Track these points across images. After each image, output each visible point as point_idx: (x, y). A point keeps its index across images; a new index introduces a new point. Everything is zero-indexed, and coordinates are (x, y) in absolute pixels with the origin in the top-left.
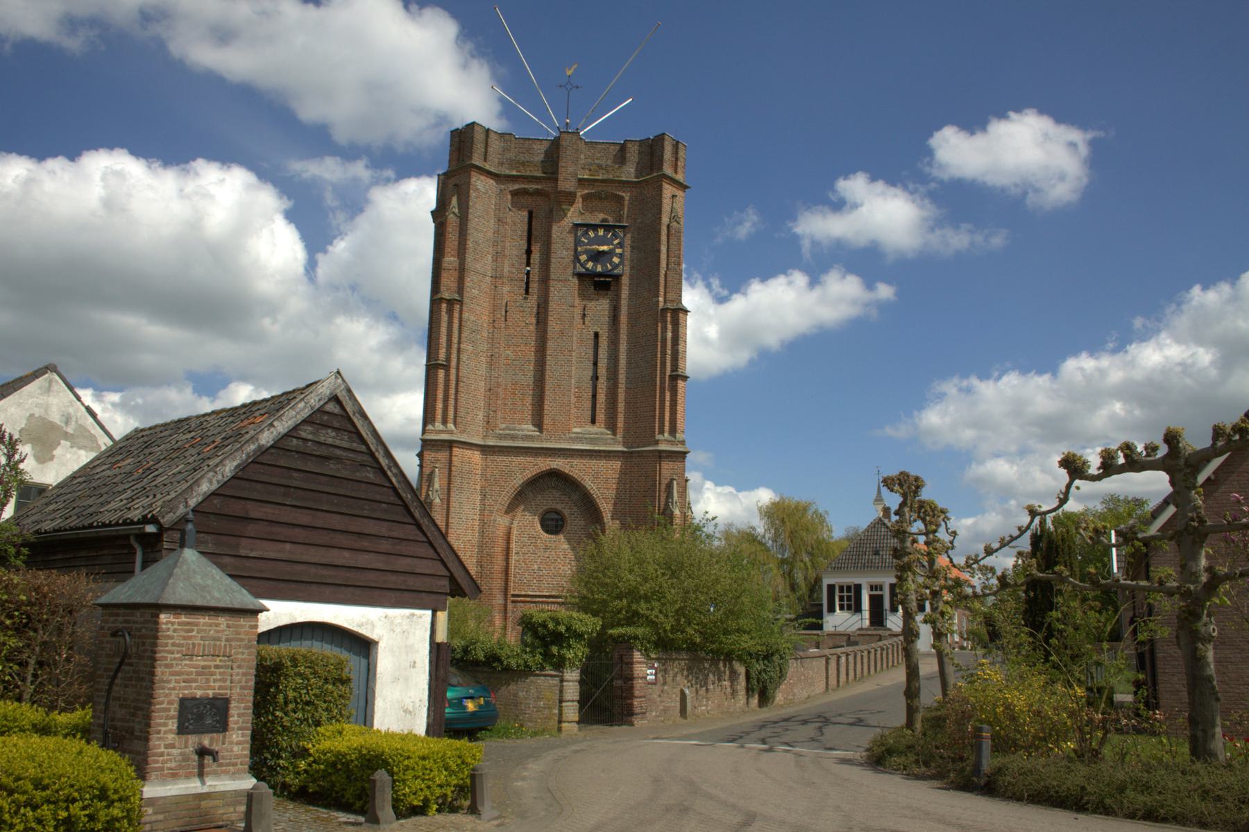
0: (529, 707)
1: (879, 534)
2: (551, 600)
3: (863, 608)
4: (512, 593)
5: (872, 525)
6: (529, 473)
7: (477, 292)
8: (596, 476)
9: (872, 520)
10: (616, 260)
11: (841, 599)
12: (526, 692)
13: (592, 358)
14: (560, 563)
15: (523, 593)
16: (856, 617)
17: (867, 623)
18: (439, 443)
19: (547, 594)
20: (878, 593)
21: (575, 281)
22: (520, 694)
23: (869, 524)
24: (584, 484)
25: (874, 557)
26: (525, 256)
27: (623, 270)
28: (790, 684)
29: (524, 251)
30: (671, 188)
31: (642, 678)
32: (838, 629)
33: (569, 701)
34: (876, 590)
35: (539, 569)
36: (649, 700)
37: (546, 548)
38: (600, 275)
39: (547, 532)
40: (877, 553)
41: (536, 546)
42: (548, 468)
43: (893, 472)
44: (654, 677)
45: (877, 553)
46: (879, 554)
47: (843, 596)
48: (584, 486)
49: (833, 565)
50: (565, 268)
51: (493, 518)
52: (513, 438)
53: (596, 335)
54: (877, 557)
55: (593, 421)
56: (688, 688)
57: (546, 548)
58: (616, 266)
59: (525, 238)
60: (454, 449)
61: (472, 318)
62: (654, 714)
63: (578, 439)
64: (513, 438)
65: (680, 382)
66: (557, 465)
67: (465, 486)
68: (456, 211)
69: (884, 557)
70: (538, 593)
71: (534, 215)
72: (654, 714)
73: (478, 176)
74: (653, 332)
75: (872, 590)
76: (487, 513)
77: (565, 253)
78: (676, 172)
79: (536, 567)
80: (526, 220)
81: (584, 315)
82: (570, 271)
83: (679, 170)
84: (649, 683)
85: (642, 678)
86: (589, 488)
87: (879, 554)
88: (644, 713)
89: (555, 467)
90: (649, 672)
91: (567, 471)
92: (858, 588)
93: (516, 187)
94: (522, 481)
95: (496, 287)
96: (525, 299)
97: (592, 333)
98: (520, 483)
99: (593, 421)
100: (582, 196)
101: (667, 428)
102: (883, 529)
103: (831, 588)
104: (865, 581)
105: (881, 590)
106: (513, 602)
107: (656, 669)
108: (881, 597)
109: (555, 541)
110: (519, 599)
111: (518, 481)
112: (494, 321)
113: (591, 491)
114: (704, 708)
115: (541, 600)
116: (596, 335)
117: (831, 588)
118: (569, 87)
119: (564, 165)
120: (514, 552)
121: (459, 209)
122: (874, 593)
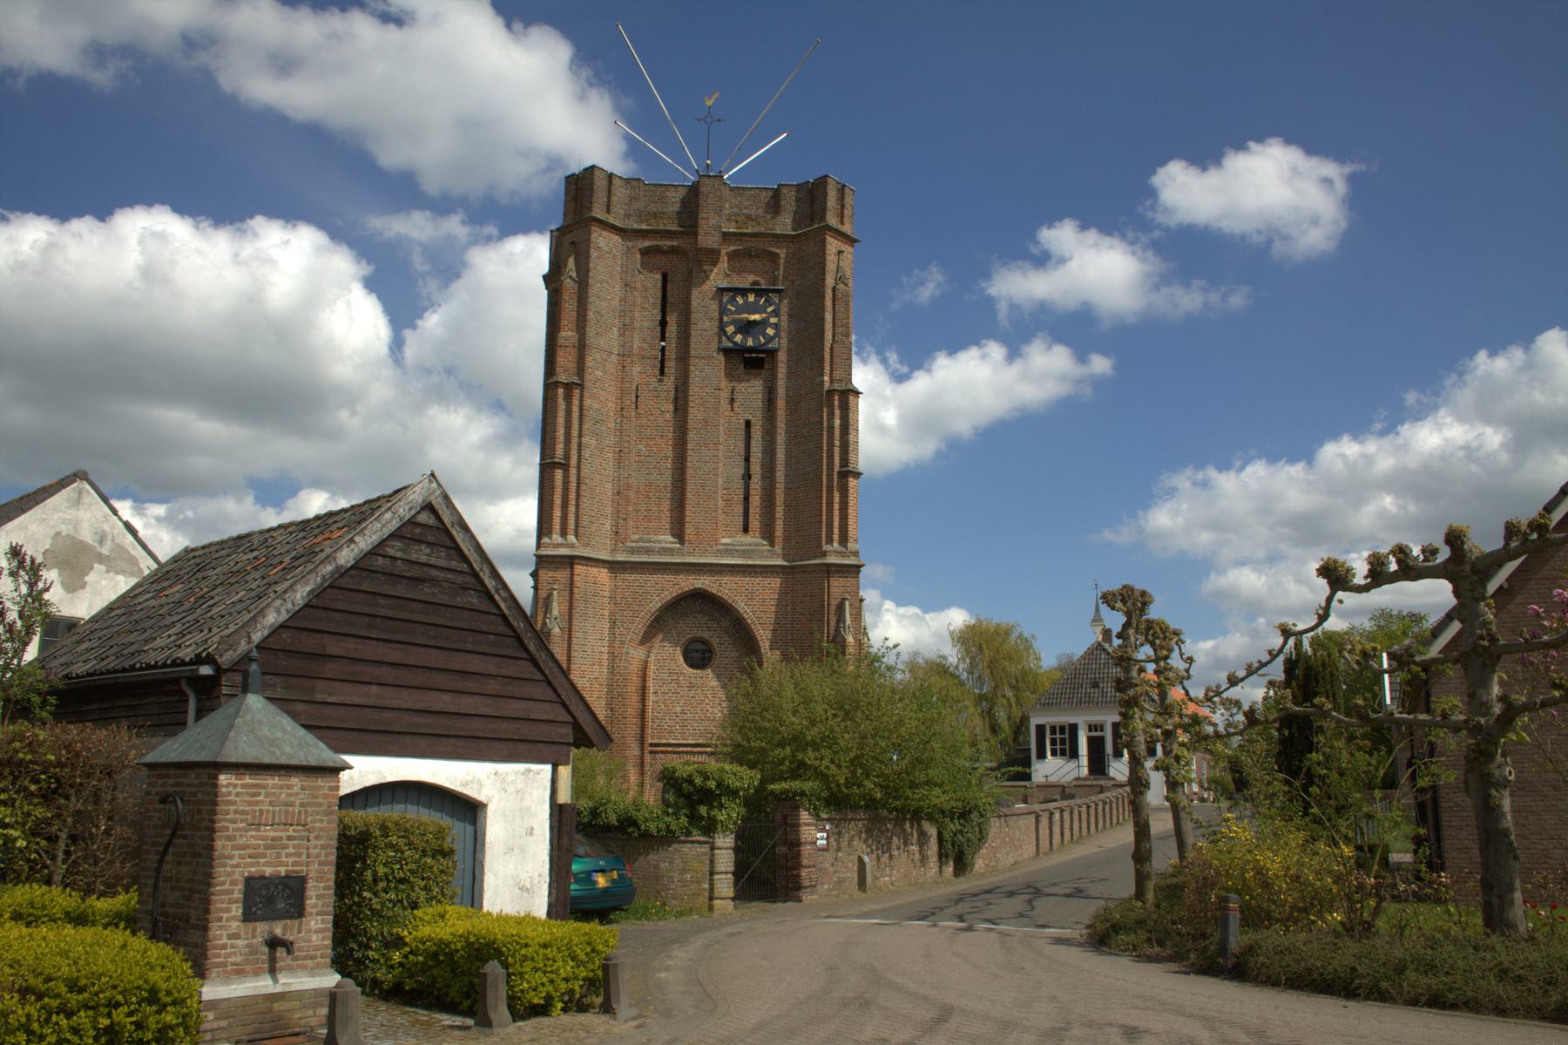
3: (1080, 753)
4: (650, 741)
6: (668, 595)
7: (601, 374)
8: (750, 597)
12: (670, 862)
15: (664, 741)
16: (1072, 764)
17: (1085, 771)
19: (693, 742)
20: (1099, 734)
21: (721, 358)
22: (662, 865)
23: (1085, 650)
26: (659, 329)
29: (658, 323)
30: (836, 242)
31: (810, 843)
32: (1050, 779)
33: (722, 873)
34: (1096, 730)
35: (683, 712)
36: (821, 869)
38: (751, 350)
39: (692, 666)
40: (1095, 685)
42: (691, 588)
44: (825, 842)
45: (1095, 685)
46: (1098, 687)
50: (708, 343)
52: (648, 551)
53: (748, 424)
54: (1096, 690)
55: (746, 530)
57: (691, 686)
59: (659, 307)
60: (576, 566)
62: (826, 887)
63: (729, 552)
64: (648, 551)
66: (703, 584)
68: (574, 274)
71: (669, 278)
72: (826, 887)
74: (818, 419)
78: (842, 222)
79: (678, 709)
81: (732, 400)
82: (714, 346)
83: (846, 220)
84: (820, 850)
85: (810, 843)
86: (742, 612)
87: (1098, 687)
88: (815, 886)
90: (819, 835)
92: (1074, 729)
93: (647, 243)
94: (660, 604)
95: (624, 367)
98: (658, 606)
99: (746, 530)
102: (1103, 656)
103: (1041, 729)
104: (1081, 720)
105: (1102, 730)
107: (827, 832)
108: (1102, 739)
110: (658, 749)
111: (655, 604)
114: (887, 879)
115: (685, 749)
117: (1041, 729)
119: (704, 216)
122: (1094, 734)
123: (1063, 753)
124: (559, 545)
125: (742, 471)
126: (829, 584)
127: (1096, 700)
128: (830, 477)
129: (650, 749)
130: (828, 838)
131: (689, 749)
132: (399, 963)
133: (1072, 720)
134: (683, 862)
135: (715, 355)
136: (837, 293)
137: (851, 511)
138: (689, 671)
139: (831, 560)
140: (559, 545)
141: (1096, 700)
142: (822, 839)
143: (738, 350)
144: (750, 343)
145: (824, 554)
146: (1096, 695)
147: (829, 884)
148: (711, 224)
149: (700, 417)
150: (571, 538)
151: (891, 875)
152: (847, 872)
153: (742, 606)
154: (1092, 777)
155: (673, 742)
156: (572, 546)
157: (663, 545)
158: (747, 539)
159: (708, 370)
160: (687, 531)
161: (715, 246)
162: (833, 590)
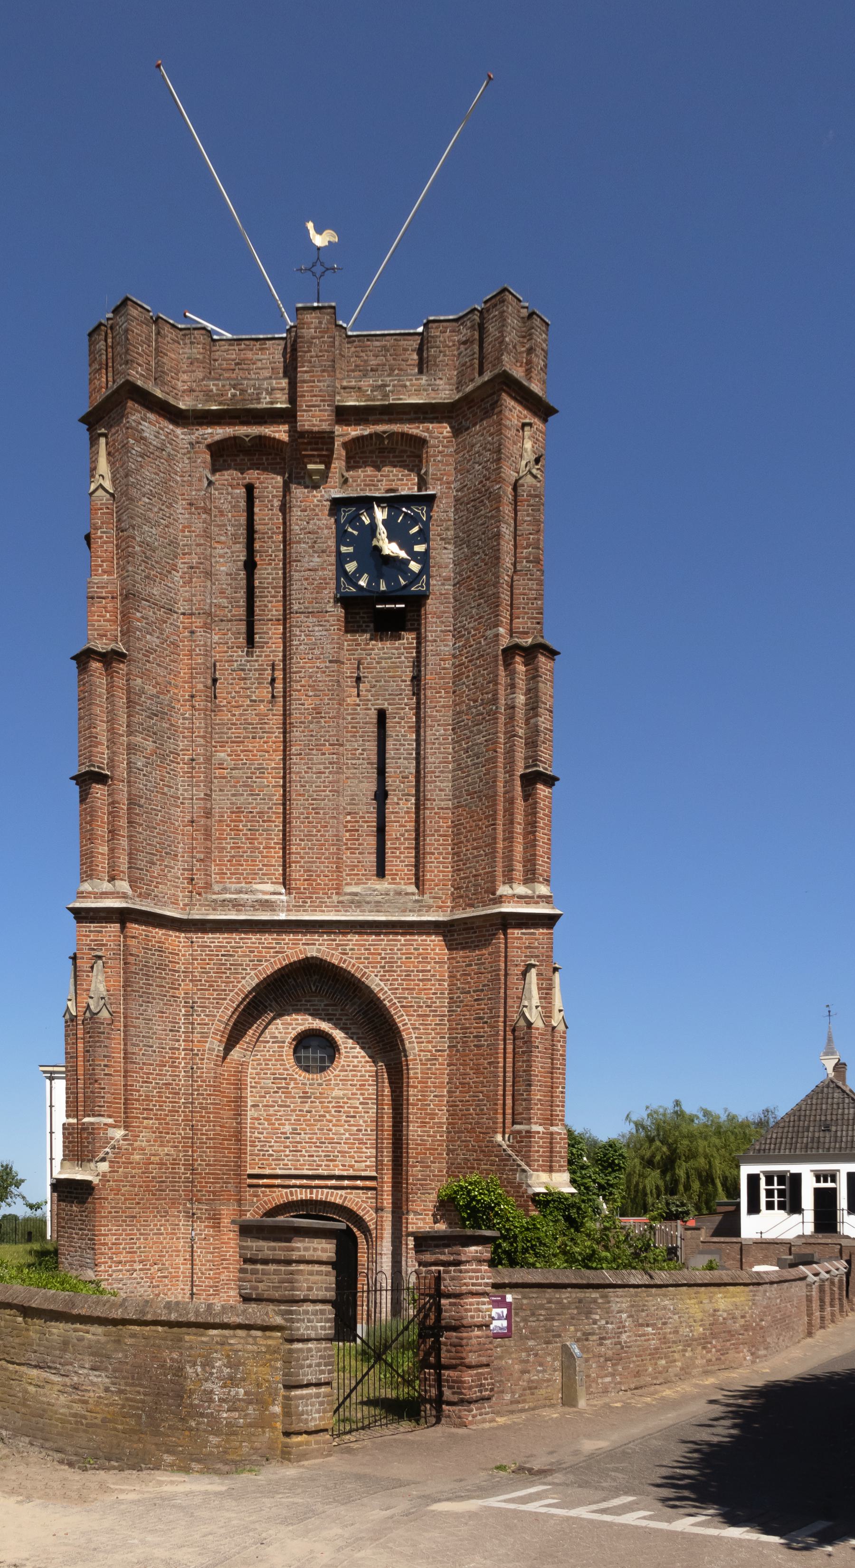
0: (211, 1400)
1: (830, 1101)
2: (317, 1182)
3: (803, 1206)
4: (249, 1171)
5: (819, 1090)
6: (268, 968)
7: (158, 641)
8: (389, 967)
9: (817, 1082)
10: (414, 566)
11: (770, 1193)
12: (203, 1366)
13: (374, 758)
14: (331, 1121)
15: (267, 1172)
16: (796, 1217)
17: (809, 1229)
18: (102, 914)
19: (310, 1173)
20: (830, 1185)
21: (340, 612)
22: (189, 1370)
23: (813, 1087)
24: (367, 982)
25: (822, 1134)
26: (243, 574)
27: (428, 584)
28: (762, 1328)
29: (241, 564)
30: (519, 408)
31: (480, 1327)
32: (765, 1236)
33: (308, 1385)
34: (826, 1181)
35: (295, 1132)
36: (498, 1369)
37: (305, 1097)
38: (385, 598)
39: (307, 1069)
40: (827, 1129)
41: (287, 1093)
42: (302, 956)
43: (704, 1107)
44: (504, 1323)
45: (827, 1129)
46: (829, 1131)
47: (773, 1190)
48: (368, 987)
49: (757, 1147)
50: (320, 589)
51: (207, 1045)
52: (237, 905)
53: (382, 715)
54: (827, 1134)
55: (381, 872)
56: (578, 1340)
57: (305, 1097)
58: (416, 577)
59: (243, 539)
60: (128, 925)
61: (151, 690)
62: (508, 1397)
63: (357, 902)
64: (237, 905)
65: (542, 790)
66: (318, 950)
67: (155, 990)
68: (107, 484)
69: (839, 1134)
70: (293, 1172)
71: (257, 493)
72: (508, 1397)
73: (144, 411)
74: (488, 840)
75: (818, 1181)
76: (197, 1037)
77: (316, 559)
78: (529, 379)
79: (288, 1128)
80: (243, 504)
81: (358, 679)
82: (329, 593)
83: (534, 373)
84: (497, 1336)
85: (480, 1327)
86: (376, 990)
87: (829, 1131)
88: (488, 1399)
89: (315, 954)
90: (495, 1312)
91: (335, 962)
92: (796, 1179)
93: (220, 432)
94: (256, 981)
95: (192, 632)
96: (248, 654)
97: (373, 714)
98: (254, 983)
99: (381, 872)
100: (345, 445)
101: (519, 867)
102: (836, 1095)
103: (753, 1180)
104: (806, 1171)
105: (834, 1180)
106: (250, 1186)
107: (509, 1306)
108: (833, 1191)
109: (321, 1085)
110: (261, 1182)
111: (250, 981)
112: (192, 696)
113: (380, 995)
114: (608, 1379)
115: (298, 1182)
116: (382, 715)
117: (753, 1180)
118: (318, 269)
119: (306, 377)
120: (250, 1103)
121: (114, 481)
122: (822, 1185)
123: (782, 1206)
124: (104, 895)
125: (373, 787)
126: (506, 939)
127: (827, 1146)
128: (509, 783)
129: (249, 1181)
130: (508, 1318)
131: (305, 1182)
132: (664, 1173)
133: (794, 1168)
134: (229, 1365)
135: (330, 607)
136: (519, 490)
137: (541, 836)
138: (302, 1076)
139: (507, 908)
140: (104, 895)
141: (827, 1146)
142: (500, 1318)
143: (363, 598)
144: (383, 587)
145: (499, 900)
146: (827, 1140)
147: (513, 1393)
148: (316, 391)
149: (309, 703)
150: (123, 886)
151: (613, 1375)
152: (544, 1371)
153: (375, 982)
154: (816, 1235)
155: (279, 1172)
156: (124, 896)
157: (260, 896)
158: (383, 886)
159: (318, 632)
160: (294, 875)
161: (325, 427)
162: (512, 953)
